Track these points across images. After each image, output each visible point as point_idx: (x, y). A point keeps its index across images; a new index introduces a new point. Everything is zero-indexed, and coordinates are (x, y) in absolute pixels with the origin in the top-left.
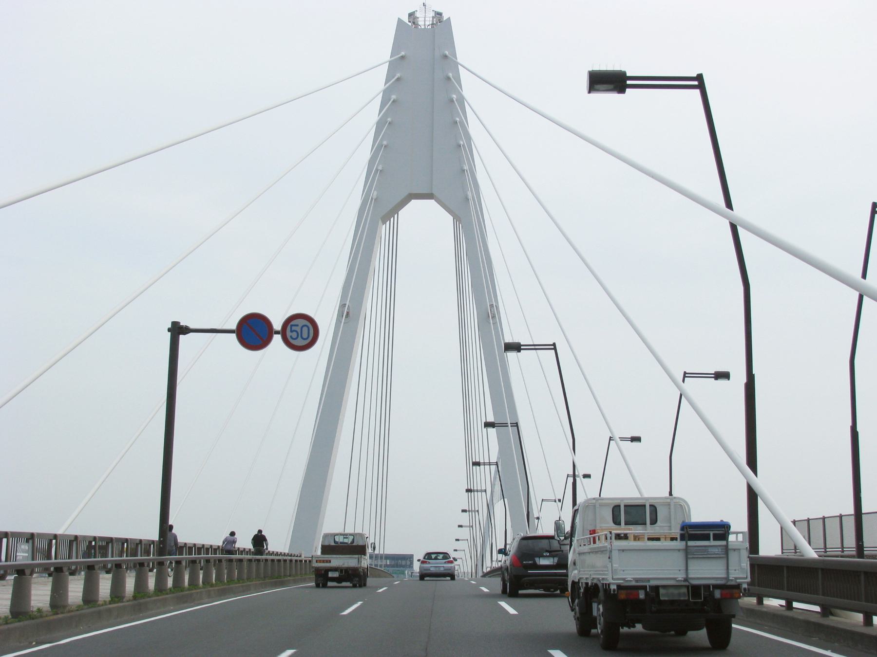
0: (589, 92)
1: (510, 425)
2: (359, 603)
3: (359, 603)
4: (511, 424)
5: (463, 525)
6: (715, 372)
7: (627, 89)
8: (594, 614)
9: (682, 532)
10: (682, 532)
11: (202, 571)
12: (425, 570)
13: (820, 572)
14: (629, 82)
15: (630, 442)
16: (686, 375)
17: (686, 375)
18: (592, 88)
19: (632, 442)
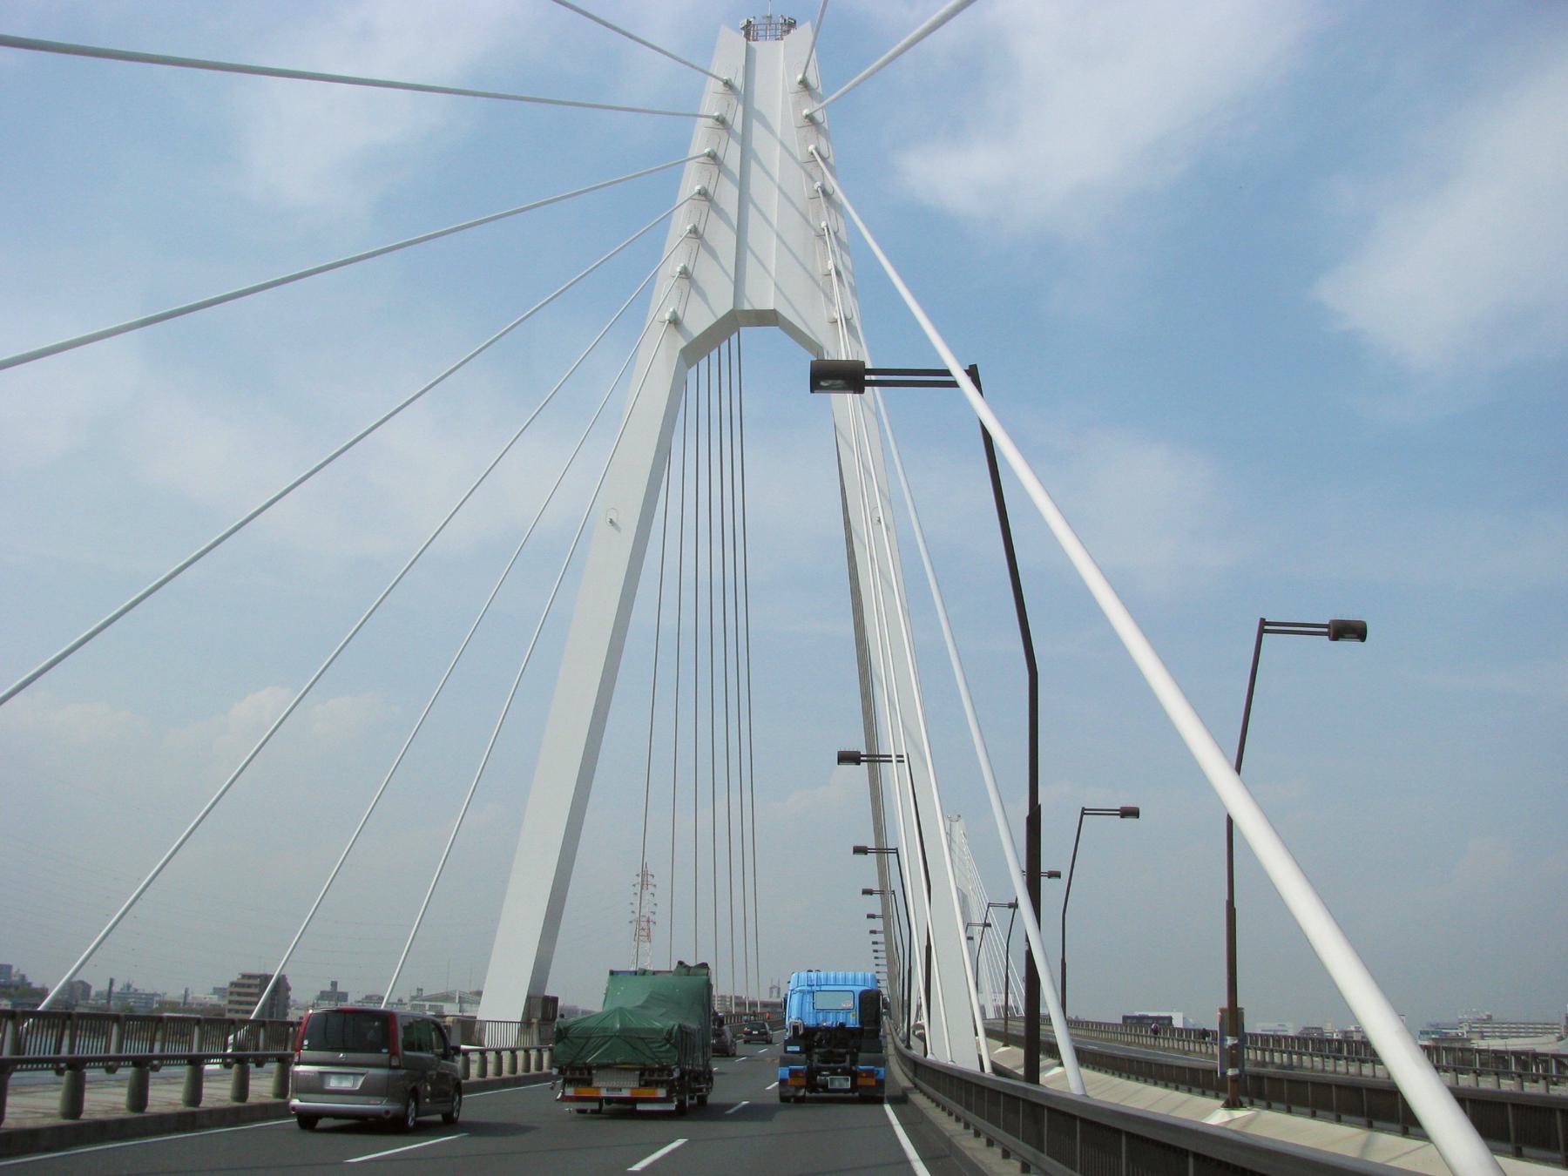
0: (812, 391)
1: (894, 758)
2: (637, 1167)
3: (637, 1167)
4: (891, 761)
5: (1007, 908)
6: (1333, 622)
7: (866, 388)
8: (674, 1108)
9: (589, 1111)
10: (589, 1111)
11: (874, 1083)
12: (219, 1100)
13: (1201, 1072)
14: (867, 378)
15: (1119, 817)
16: (1266, 627)
17: (1266, 627)
18: (815, 386)
19: (1122, 817)
